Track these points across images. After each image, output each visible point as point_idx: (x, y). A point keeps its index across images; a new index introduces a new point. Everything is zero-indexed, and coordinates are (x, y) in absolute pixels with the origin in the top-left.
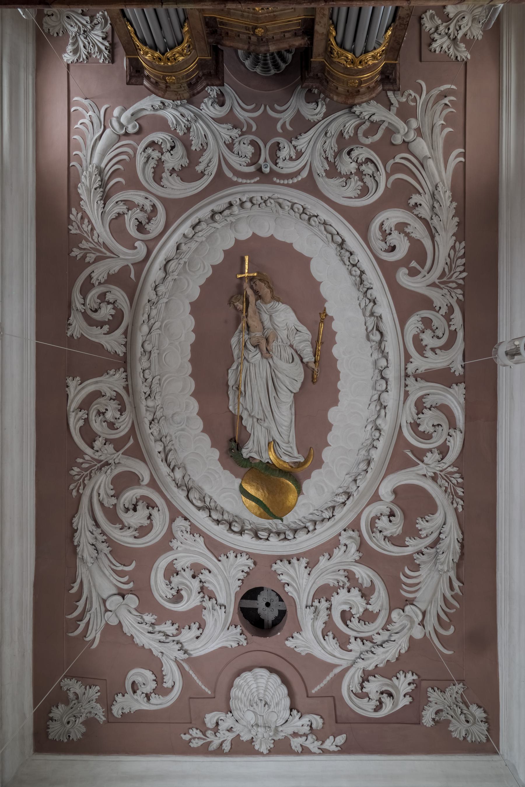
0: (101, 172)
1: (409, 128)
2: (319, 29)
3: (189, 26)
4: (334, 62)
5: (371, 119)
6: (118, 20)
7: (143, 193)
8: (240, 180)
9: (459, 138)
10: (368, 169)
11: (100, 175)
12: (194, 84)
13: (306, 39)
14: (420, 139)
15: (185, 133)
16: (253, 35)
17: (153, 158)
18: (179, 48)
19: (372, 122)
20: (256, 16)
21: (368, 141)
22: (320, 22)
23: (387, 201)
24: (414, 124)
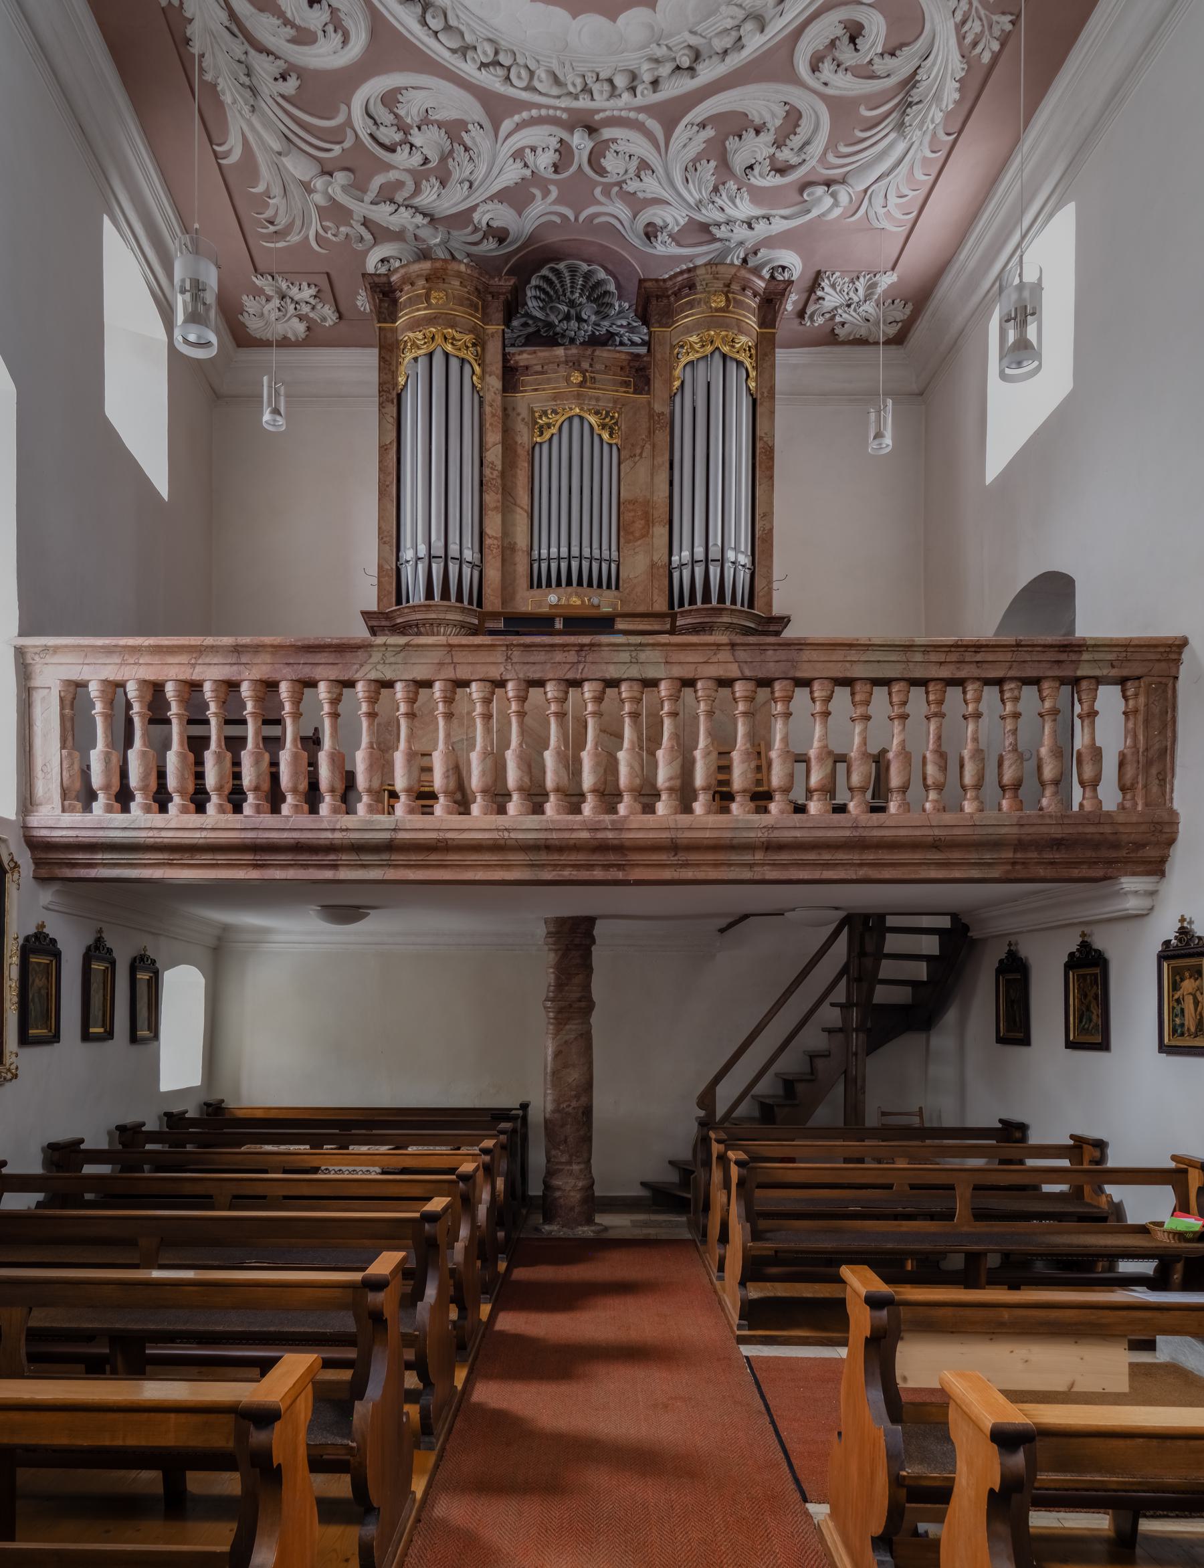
0: (900, 126)
1: (326, 193)
2: (495, 383)
3: (671, 385)
4: (471, 332)
7: (829, 91)
8: (632, 115)
9: (234, 182)
10: (389, 135)
11: (903, 123)
14: (306, 179)
15: (724, 184)
18: (691, 357)
19: (392, 201)
21: (393, 175)
23: (345, 82)
24: (319, 198)
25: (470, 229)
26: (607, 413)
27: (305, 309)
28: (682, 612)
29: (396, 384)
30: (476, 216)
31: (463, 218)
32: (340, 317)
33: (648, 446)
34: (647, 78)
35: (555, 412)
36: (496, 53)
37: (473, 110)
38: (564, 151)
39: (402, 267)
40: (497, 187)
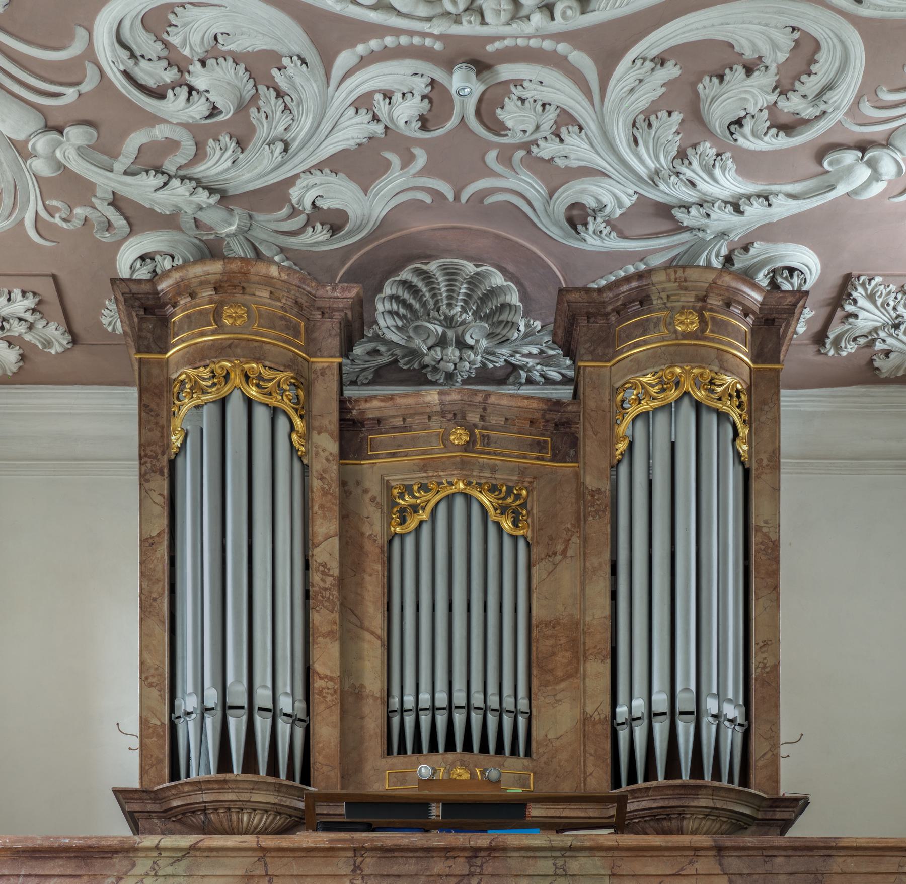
1: (52, 157)
3: (612, 448)
4: (287, 367)
5: (164, 178)
6: (765, 462)
8: (547, 45)
10: (154, 73)
12: (634, 301)
13: (354, 412)
15: (694, 146)
16: (475, 426)
17: (804, 96)
18: (644, 407)
19: (159, 170)
20: (464, 472)
21: (160, 132)
22: (328, 460)
25: (285, 211)
26: (510, 491)
29: (168, 445)
30: (295, 193)
32: (75, 341)
35: (424, 488)
38: (437, 96)
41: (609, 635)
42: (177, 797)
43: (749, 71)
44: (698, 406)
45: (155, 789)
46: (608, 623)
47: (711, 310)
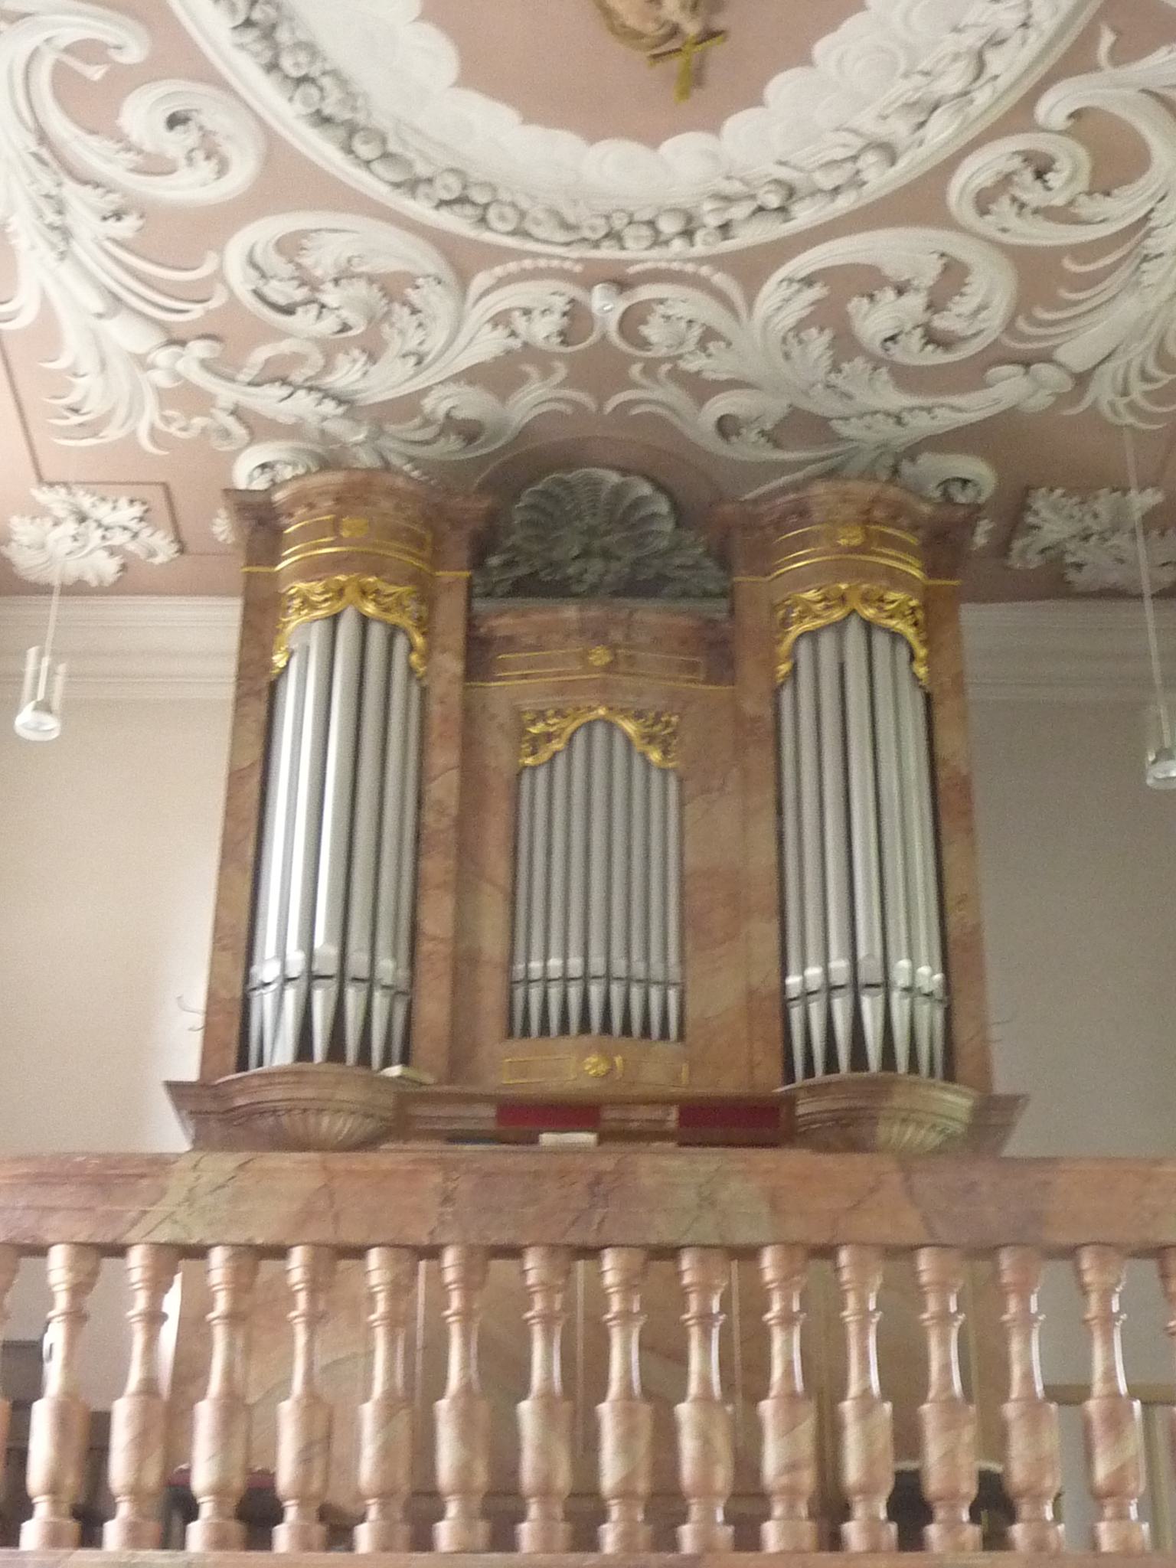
2: (452, 664)
7: (1005, 238)
8: (690, 268)
10: (282, 291)
13: (482, 630)
18: (808, 625)
19: (284, 381)
21: (285, 347)
25: (417, 421)
26: (658, 716)
27: (119, 538)
28: (810, 1089)
29: (270, 665)
30: (428, 403)
31: (407, 406)
32: (182, 551)
33: (735, 772)
34: (713, 221)
35: (558, 713)
36: (465, 187)
37: (425, 260)
38: (577, 317)
39: (295, 478)
40: (464, 362)
41: (774, 887)
42: (242, 1092)
43: (901, 291)
44: (868, 626)
45: (587, 1138)
46: (774, 873)
47: (876, 523)
